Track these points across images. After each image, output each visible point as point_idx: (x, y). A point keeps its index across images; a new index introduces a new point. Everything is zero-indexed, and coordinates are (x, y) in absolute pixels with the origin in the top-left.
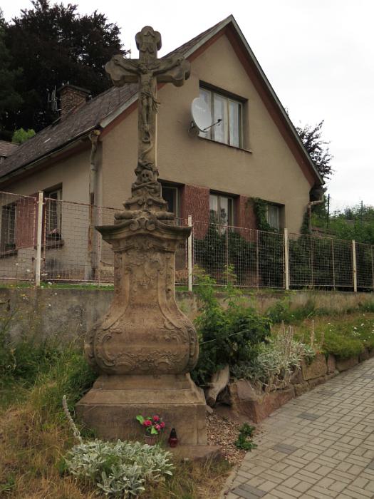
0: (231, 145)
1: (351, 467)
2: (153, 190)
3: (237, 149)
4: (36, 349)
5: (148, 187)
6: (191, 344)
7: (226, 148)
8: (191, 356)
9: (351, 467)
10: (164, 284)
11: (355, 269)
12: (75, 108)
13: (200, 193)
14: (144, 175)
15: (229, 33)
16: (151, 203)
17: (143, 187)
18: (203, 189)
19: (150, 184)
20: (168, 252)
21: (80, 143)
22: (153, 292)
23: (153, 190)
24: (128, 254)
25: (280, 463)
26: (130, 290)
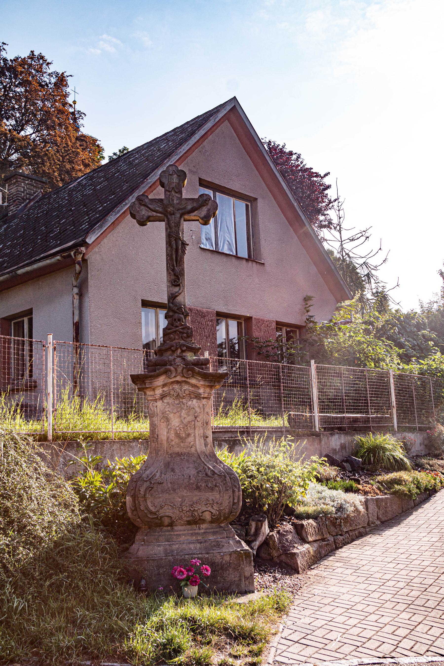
0: (239, 255)
1: (437, 591)
2: (185, 335)
3: (247, 260)
4: (298, 507)
5: (180, 332)
6: (234, 491)
7: (234, 260)
8: (234, 504)
9: (437, 591)
10: (202, 431)
11: (394, 404)
12: (29, 203)
13: (204, 316)
14: (175, 320)
15: (235, 97)
16: (185, 348)
17: (175, 332)
18: (208, 312)
19: (182, 329)
20: (204, 398)
21: (58, 260)
22: (191, 439)
23: (185, 335)
24: (163, 402)
25: (327, 605)
26: (168, 439)
